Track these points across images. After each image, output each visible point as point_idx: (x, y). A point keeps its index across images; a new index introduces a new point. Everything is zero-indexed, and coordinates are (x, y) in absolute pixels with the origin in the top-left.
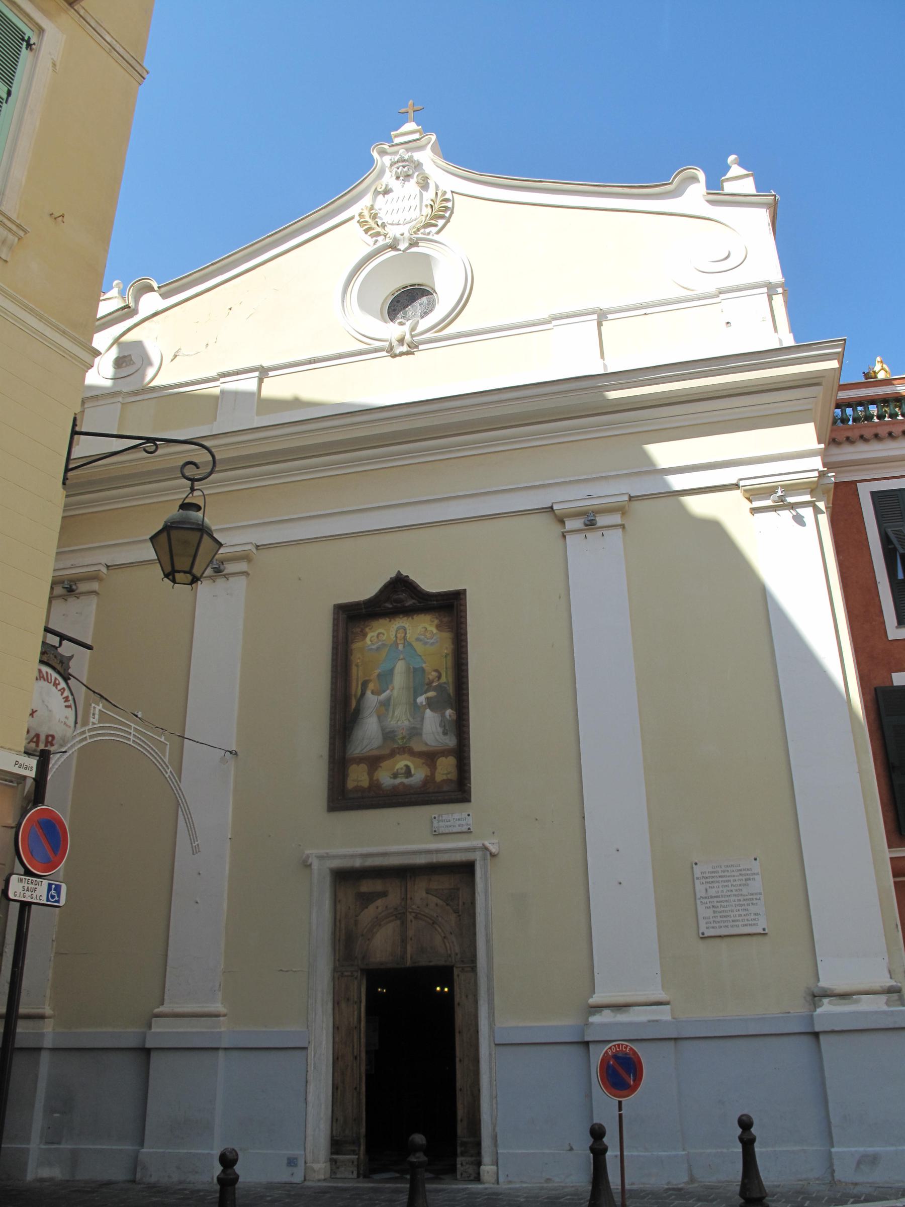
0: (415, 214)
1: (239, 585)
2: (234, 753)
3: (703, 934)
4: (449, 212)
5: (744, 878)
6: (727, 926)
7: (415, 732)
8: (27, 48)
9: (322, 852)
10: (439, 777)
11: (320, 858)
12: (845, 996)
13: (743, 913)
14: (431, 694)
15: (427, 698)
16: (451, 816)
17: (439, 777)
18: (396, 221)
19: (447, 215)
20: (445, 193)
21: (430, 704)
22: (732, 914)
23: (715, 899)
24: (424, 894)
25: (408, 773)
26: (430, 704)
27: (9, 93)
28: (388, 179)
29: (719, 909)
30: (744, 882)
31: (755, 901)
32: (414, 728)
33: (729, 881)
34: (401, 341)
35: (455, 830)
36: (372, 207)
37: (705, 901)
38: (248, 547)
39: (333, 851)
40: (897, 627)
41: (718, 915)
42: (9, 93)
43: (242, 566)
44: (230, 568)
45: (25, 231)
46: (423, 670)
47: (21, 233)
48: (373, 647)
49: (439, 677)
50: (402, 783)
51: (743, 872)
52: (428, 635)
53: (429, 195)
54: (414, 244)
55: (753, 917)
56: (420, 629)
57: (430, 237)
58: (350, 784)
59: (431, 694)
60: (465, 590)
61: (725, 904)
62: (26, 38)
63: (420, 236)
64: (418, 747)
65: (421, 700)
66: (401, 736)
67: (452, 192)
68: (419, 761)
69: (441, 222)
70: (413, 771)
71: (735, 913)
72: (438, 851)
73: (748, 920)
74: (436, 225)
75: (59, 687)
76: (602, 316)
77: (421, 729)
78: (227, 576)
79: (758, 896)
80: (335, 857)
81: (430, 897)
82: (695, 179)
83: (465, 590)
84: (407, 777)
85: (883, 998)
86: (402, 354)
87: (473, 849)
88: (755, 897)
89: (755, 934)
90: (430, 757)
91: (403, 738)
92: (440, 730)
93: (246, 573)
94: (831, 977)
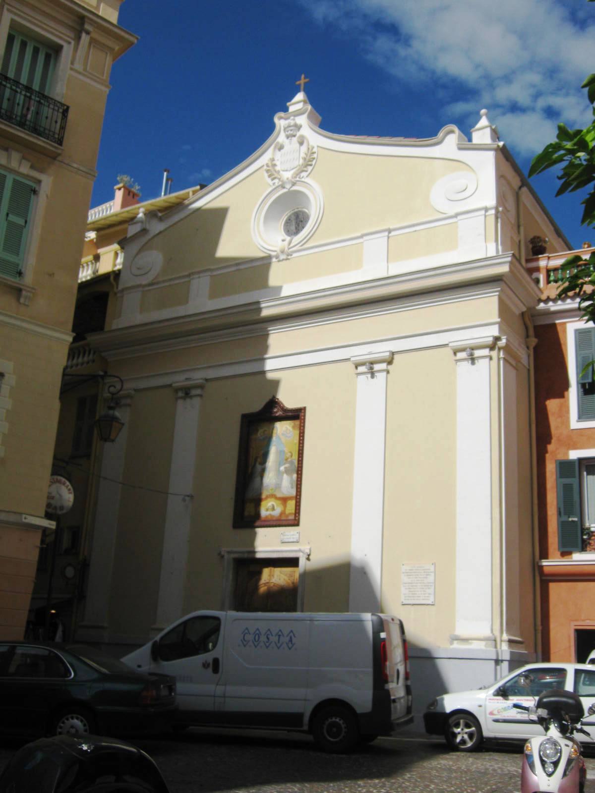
0: (296, 163)
1: (196, 401)
2: (191, 497)
3: (402, 602)
4: (314, 161)
5: (426, 574)
6: (414, 599)
7: (278, 486)
8: (34, 194)
9: (229, 549)
10: (287, 512)
11: (229, 552)
12: (465, 640)
13: (423, 592)
14: (287, 465)
15: (285, 468)
16: (290, 532)
17: (287, 512)
18: (286, 169)
19: (313, 163)
20: (313, 148)
21: (287, 471)
22: (417, 593)
23: (410, 585)
24: (279, 573)
25: (273, 509)
26: (287, 471)
27: (26, 222)
28: (282, 138)
29: (412, 590)
30: (425, 576)
31: (429, 587)
32: (278, 484)
33: (418, 575)
34: (282, 252)
35: (290, 540)
36: (273, 160)
37: (405, 585)
38: (201, 381)
39: (235, 549)
40: (578, 421)
41: (411, 593)
42: (26, 222)
43: (198, 392)
44: (193, 392)
45: (34, 289)
46: (284, 452)
47: (34, 291)
48: (261, 438)
49: (291, 456)
50: (270, 515)
51: (426, 571)
52: (288, 432)
53: (304, 149)
54: (294, 184)
55: (427, 595)
56: (284, 429)
57: (303, 180)
58: (246, 514)
59: (287, 465)
60: (305, 408)
61: (415, 587)
62: (33, 189)
63: (298, 179)
64: (279, 495)
65: (282, 468)
66: (271, 488)
67: (318, 146)
68: (279, 502)
69: (310, 168)
70: (275, 508)
71: (419, 593)
72: (282, 551)
73: (425, 597)
74: (306, 171)
75: (66, 485)
76: (390, 231)
77: (281, 484)
78: (191, 397)
79: (431, 584)
80: (236, 552)
81: (282, 575)
82: (452, 132)
83: (305, 408)
84: (272, 511)
85: (483, 643)
86: (283, 260)
87: (300, 551)
88: (429, 585)
89: (428, 605)
90: (284, 500)
91: (272, 490)
92: (290, 486)
93: (201, 396)
94: (461, 630)
